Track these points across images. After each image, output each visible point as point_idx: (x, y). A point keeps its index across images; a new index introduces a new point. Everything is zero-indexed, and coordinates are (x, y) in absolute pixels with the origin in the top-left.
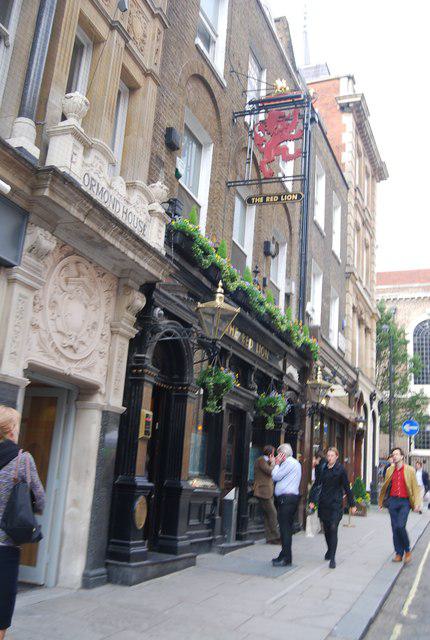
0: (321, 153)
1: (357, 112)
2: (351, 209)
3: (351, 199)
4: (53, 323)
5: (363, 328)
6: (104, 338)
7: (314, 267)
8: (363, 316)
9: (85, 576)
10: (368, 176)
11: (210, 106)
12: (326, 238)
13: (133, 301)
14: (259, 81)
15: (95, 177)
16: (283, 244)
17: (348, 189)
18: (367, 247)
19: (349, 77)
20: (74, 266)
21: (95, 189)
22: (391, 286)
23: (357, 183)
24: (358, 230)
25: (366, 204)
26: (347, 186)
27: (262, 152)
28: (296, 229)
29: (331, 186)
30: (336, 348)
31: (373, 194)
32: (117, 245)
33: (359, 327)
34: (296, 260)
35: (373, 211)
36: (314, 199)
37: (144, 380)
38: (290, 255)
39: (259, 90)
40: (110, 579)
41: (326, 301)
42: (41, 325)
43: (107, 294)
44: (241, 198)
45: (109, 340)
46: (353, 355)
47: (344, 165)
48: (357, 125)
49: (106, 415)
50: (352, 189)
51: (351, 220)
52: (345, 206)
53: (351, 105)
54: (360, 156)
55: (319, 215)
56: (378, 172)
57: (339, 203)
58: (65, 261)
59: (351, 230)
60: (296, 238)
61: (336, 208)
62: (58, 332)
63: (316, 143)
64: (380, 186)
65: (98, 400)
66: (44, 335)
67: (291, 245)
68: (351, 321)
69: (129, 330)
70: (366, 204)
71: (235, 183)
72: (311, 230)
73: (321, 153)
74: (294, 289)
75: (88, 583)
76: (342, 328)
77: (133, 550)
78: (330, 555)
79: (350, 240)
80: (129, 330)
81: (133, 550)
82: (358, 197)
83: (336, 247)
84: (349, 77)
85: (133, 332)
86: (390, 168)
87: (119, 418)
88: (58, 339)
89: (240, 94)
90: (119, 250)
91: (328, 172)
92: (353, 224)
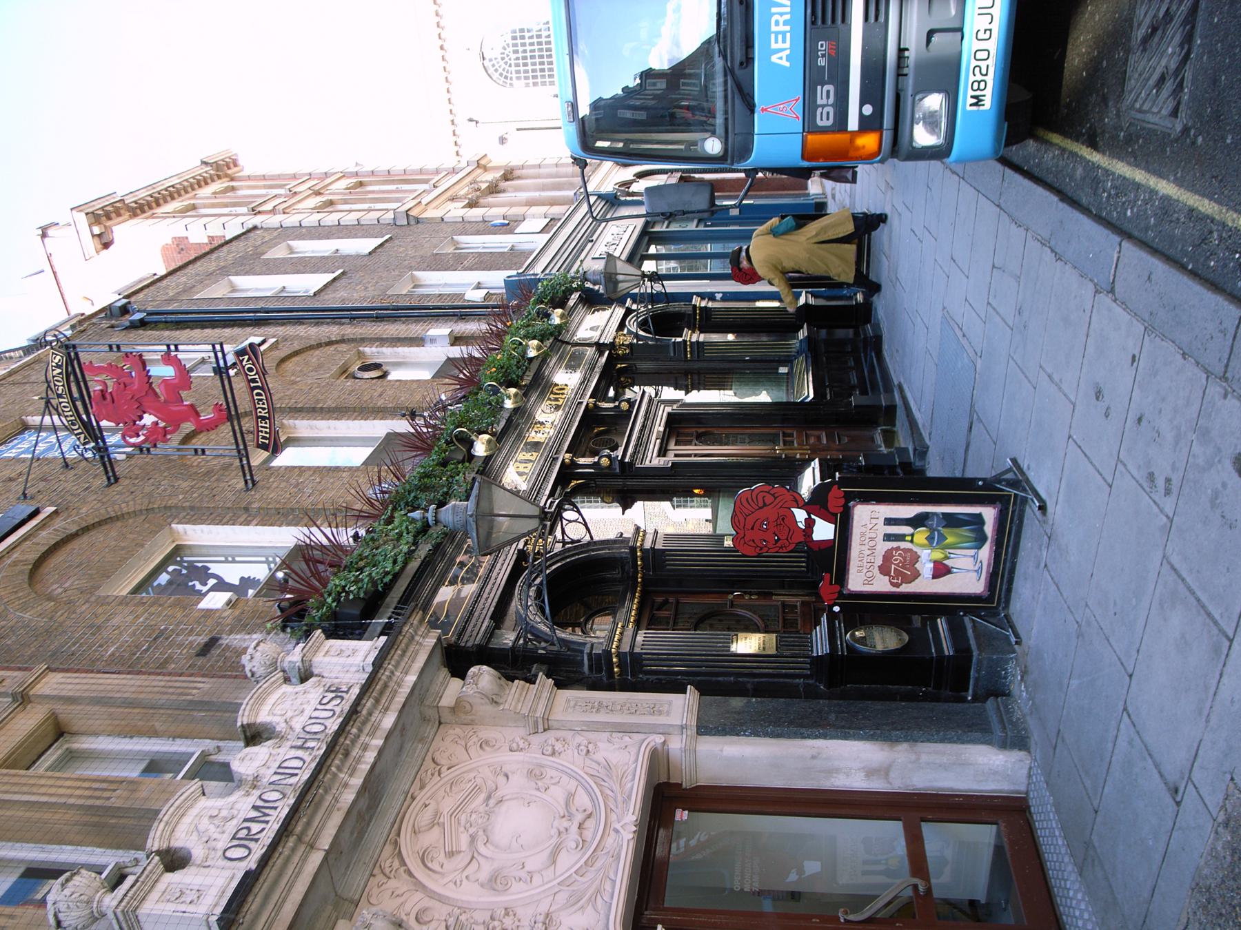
0: (188, 289)
1: (109, 218)
2: (291, 220)
3: (274, 221)
4: (537, 879)
5: (503, 185)
6: (558, 746)
7: (401, 290)
8: (484, 186)
9: (1004, 745)
10: (233, 189)
11: (97, 536)
12: (345, 268)
13: (484, 695)
14: (40, 428)
15: (231, 827)
16: (360, 355)
17: (255, 228)
18: (361, 184)
19: (44, 235)
20: (421, 836)
21: (255, 828)
22: (720, 679)
23: (244, 210)
24: (331, 203)
25: (281, 191)
26: (249, 231)
27: (177, 427)
28: (333, 331)
29: (254, 264)
30: (546, 237)
31: (264, 178)
32: (370, 756)
33: (504, 191)
34: (392, 329)
35: (294, 177)
36: (276, 298)
37: (631, 653)
38: (383, 341)
39: (55, 429)
40: (997, 690)
41: (459, 261)
42: (543, 908)
43: (474, 750)
44: (269, 460)
45: (559, 734)
46: (553, 202)
47: (211, 238)
48: (135, 215)
49: (704, 728)
50: (257, 220)
51: (312, 220)
52: (286, 233)
53: (97, 230)
54: (194, 207)
55: (306, 284)
56: (222, 169)
57: (224, 282)
58: (413, 864)
59: (330, 219)
60: (349, 330)
61: (291, 250)
62: (554, 862)
63: (170, 301)
64: (249, 166)
65: (676, 745)
66: (562, 898)
67: (363, 340)
68: (494, 211)
69: (538, 697)
70: (281, 191)
71: (247, 471)
72: (333, 300)
73: (188, 289)
74: (441, 331)
75: (1016, 740)
76: (508, 227)
77: (948, 650)
78: (1151, 273)
79: (350, 219)
80: (538, 697)
81: (948, 650)
82: (268, 207)
83: (365, 245)
84: (44, 235)
85: (545, 682)
86: (214, 151)
87: (703, 697)
88: (568, 861)
89: (72, 472)
90: (381, 752)
91: (225, 271)
92: (320, 216)
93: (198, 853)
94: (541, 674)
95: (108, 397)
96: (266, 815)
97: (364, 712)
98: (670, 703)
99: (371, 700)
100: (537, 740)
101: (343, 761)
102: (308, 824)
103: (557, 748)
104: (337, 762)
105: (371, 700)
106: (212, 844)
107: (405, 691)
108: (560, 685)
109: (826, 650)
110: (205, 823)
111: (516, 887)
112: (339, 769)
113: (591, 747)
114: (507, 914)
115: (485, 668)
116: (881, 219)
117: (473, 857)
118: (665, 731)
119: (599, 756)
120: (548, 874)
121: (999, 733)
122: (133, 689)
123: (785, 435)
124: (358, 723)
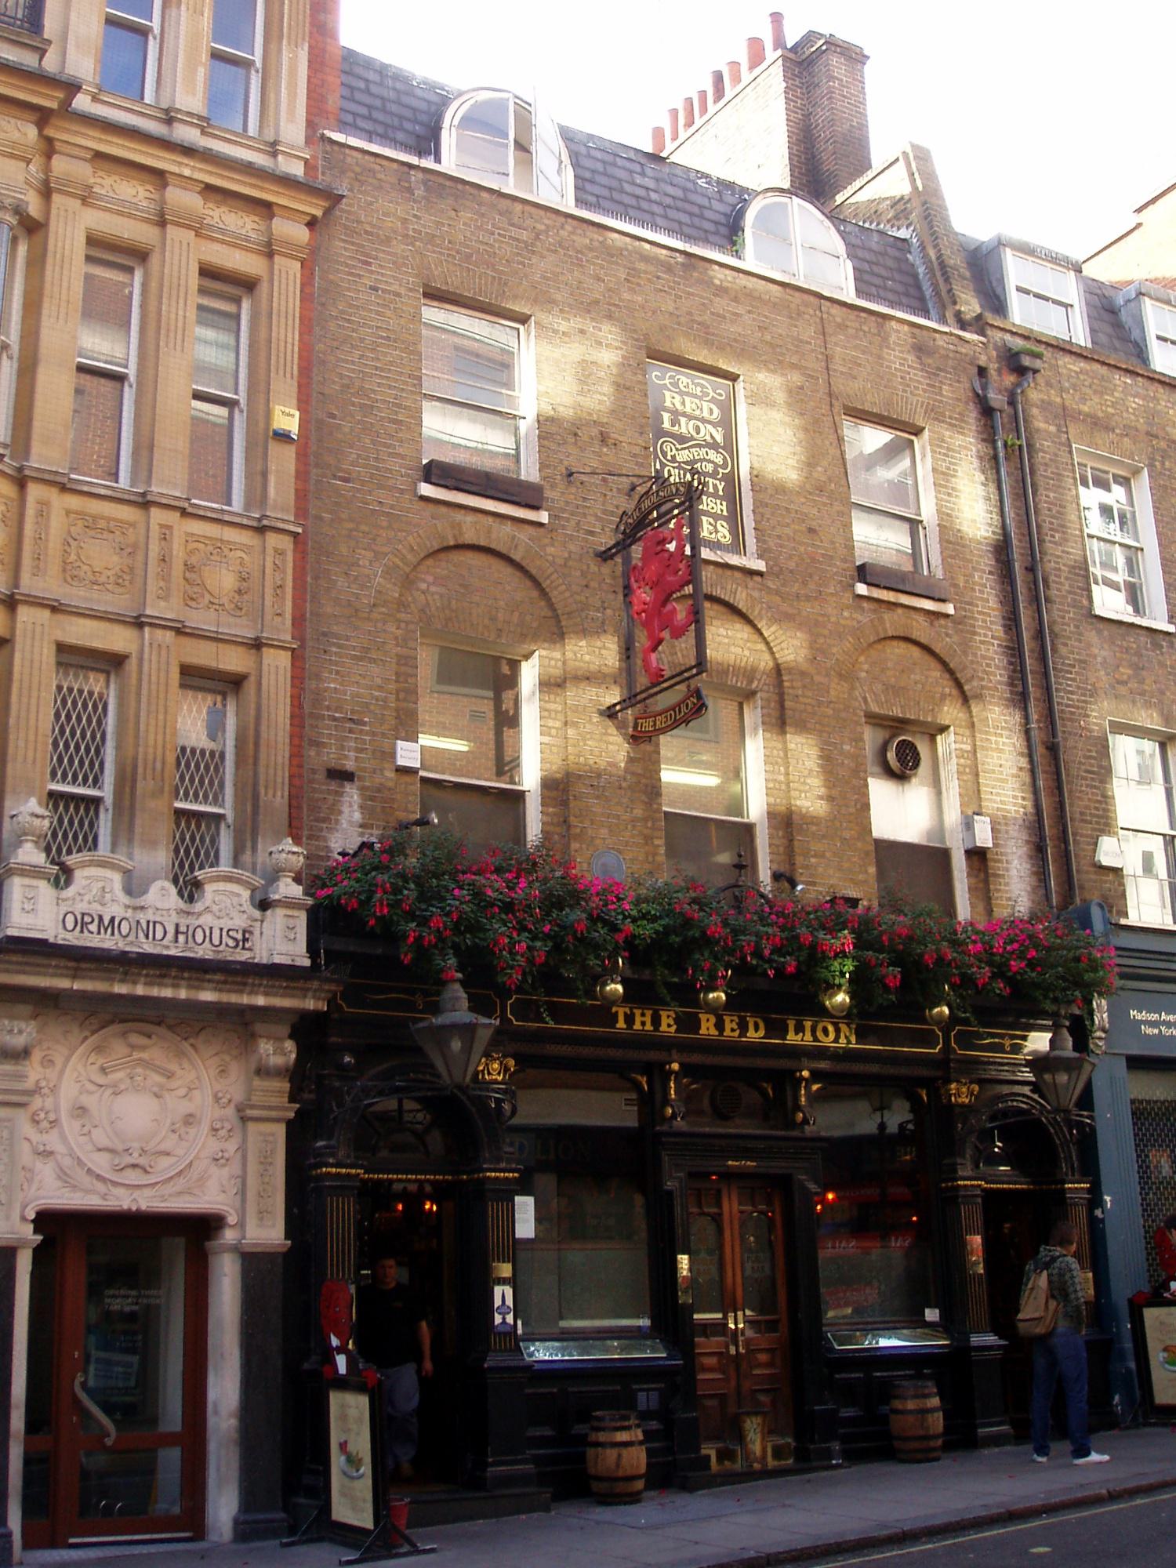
4: (82, 1139)
62: (100, 1150)
65: (229, 1236)
75: (246, 1531)
93: (70, 892)
94: (298, 1106)
95: (659, 548)
96: (106, 930)
97: (208, 977)
98: (274, 1226)
99: (223, 978)
100: (230, 1111)
101: (154, 975)
102: (91, 970)
103: (220, 1132)
104: (152, 972)
105: (223, 978)
106: (78, 898)
107: (245, 1000)
108: (290, 1124)
109: (973, 1344)
110: (96, 887)
111: (77, 1124)
112: (147, 975)
113: (222, 1161)
114: (51, 1122)
115: (293, 1056)
116: (346, 1442)
117: (101, 1086)
118: (241, 1225)
119: (214, 1170)
120: (90, 1147)
121: (242, 1518)
122: (272, 737)
123: (775, 1322)
124: (194, 975)
